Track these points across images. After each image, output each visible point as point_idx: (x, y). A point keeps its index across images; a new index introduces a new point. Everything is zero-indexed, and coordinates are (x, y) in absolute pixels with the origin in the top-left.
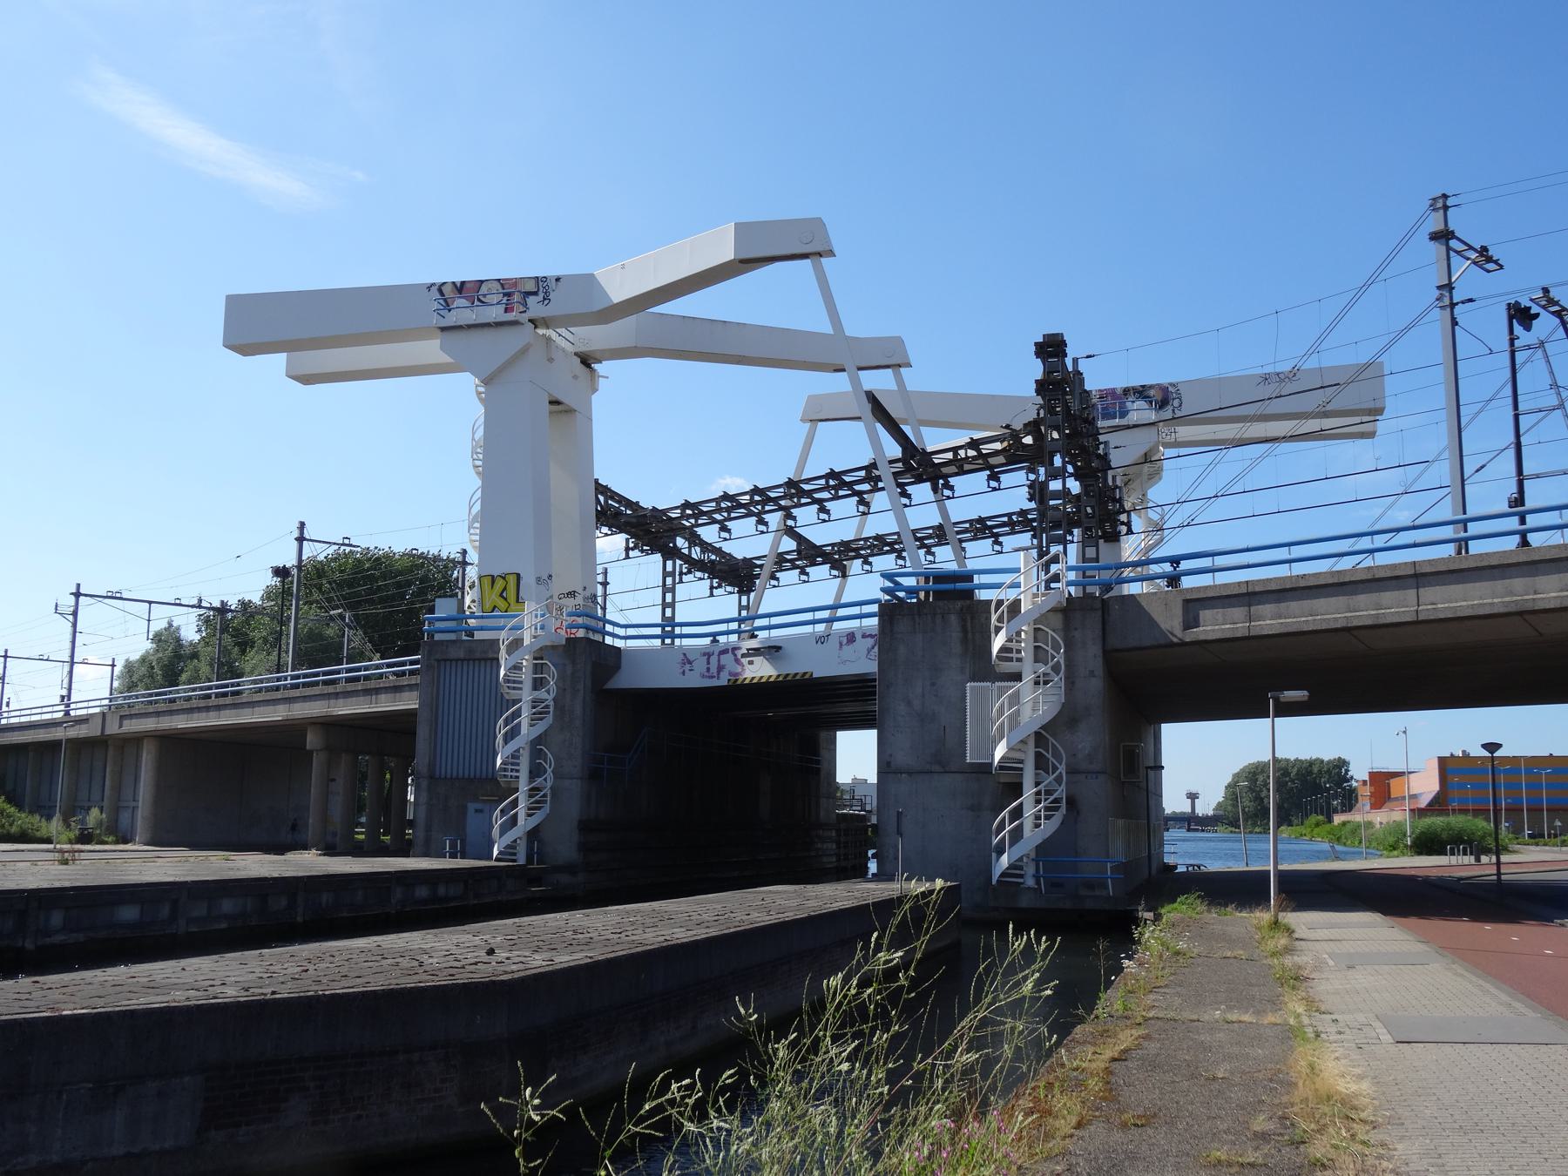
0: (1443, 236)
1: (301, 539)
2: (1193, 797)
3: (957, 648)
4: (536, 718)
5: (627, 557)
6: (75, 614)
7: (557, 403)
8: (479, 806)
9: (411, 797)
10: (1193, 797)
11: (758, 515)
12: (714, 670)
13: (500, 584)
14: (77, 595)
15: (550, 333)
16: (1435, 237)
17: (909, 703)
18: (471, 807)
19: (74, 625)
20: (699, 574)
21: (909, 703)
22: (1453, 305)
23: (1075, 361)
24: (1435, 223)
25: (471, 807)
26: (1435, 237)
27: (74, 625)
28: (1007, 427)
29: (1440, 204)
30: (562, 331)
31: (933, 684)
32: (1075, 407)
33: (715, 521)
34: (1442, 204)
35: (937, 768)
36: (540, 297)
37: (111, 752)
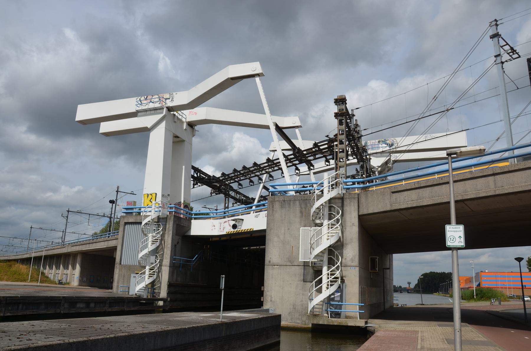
0: (496, 36)
1: (117, 191)
2: (409, 283)
3: (298, 214)
4: (153, 242)
5: (194, 187)
6: (67, 217)
7: (177, 137)
8: (135, 275)
9: (223, 286)
10: (409, 283)
11: (249, 179)
12: (222, 229)
13: (150, 197)
14: (68, 211)
15: (175, 113)
16: (493, 37)
17: (278, 237)
18: (132, 275)
19: (67, 220)
20: (238, 204)
21: (278, 237)
22: (502, 63)
23: (352, 110)
24: (492, 32)
25: (132, 275)
26: (493, 37)
27: (67, 220)
28: (327, 136)
29: (494, 23)
30: (179, 112)
31: (289, 229)
32: (352, 126)
33: (236, 182)
34: (496, 23)
35: (289, 264)
36: (170, 100)
37: (62, 258)
